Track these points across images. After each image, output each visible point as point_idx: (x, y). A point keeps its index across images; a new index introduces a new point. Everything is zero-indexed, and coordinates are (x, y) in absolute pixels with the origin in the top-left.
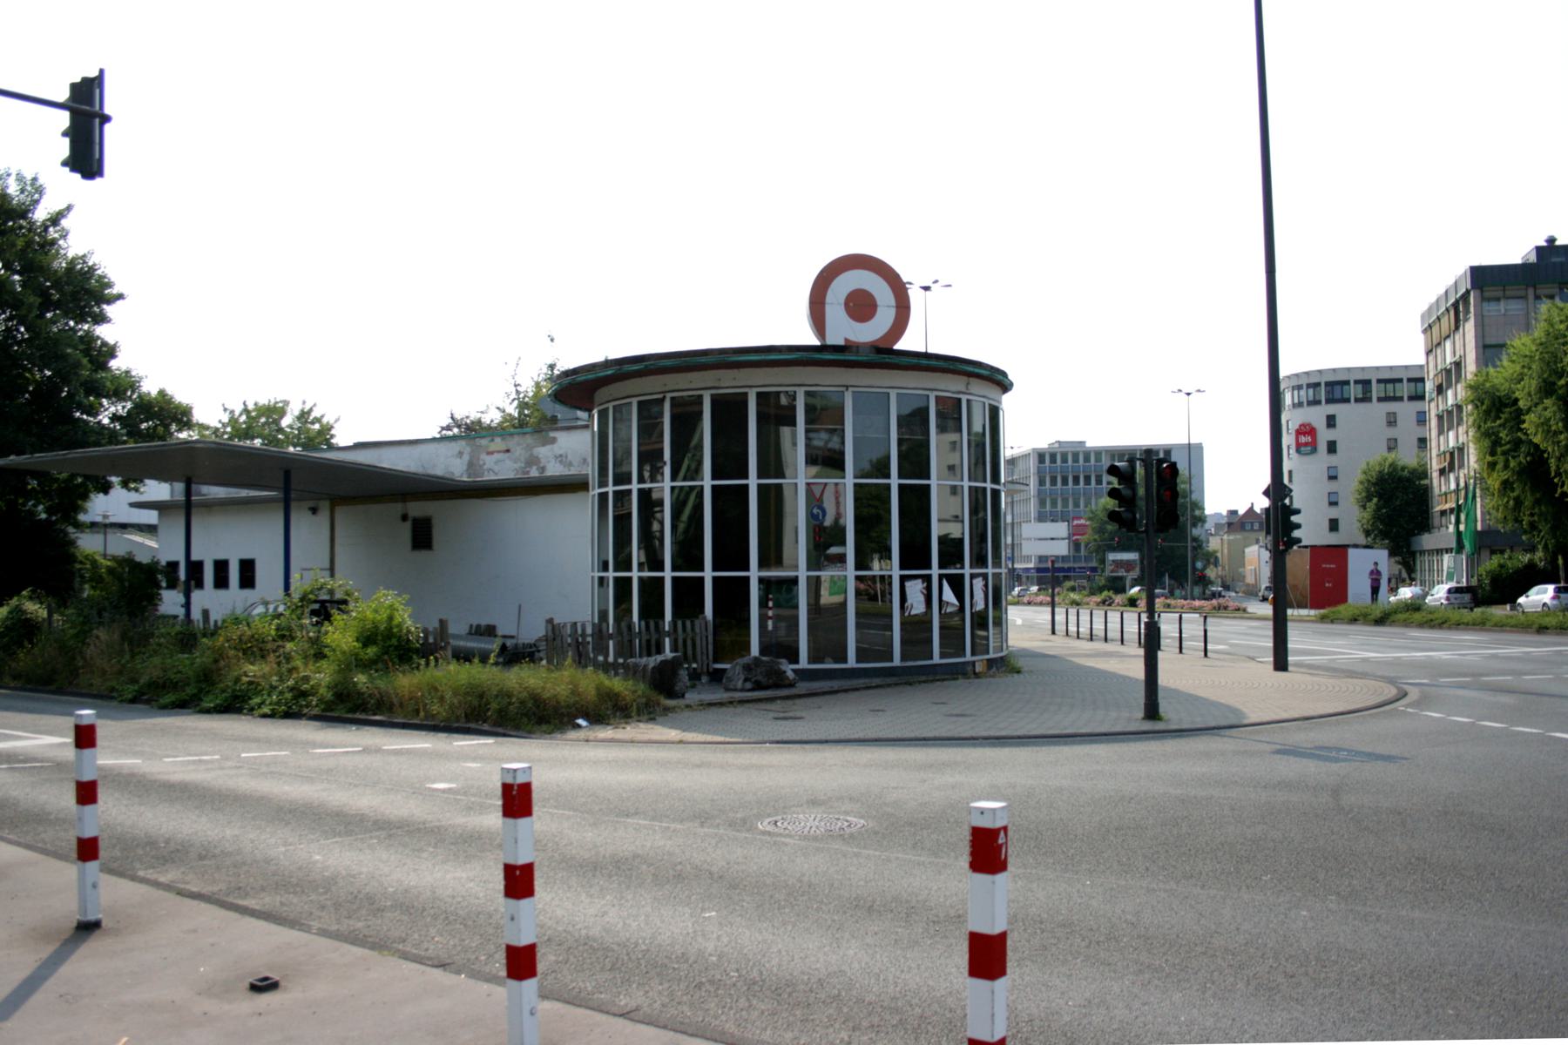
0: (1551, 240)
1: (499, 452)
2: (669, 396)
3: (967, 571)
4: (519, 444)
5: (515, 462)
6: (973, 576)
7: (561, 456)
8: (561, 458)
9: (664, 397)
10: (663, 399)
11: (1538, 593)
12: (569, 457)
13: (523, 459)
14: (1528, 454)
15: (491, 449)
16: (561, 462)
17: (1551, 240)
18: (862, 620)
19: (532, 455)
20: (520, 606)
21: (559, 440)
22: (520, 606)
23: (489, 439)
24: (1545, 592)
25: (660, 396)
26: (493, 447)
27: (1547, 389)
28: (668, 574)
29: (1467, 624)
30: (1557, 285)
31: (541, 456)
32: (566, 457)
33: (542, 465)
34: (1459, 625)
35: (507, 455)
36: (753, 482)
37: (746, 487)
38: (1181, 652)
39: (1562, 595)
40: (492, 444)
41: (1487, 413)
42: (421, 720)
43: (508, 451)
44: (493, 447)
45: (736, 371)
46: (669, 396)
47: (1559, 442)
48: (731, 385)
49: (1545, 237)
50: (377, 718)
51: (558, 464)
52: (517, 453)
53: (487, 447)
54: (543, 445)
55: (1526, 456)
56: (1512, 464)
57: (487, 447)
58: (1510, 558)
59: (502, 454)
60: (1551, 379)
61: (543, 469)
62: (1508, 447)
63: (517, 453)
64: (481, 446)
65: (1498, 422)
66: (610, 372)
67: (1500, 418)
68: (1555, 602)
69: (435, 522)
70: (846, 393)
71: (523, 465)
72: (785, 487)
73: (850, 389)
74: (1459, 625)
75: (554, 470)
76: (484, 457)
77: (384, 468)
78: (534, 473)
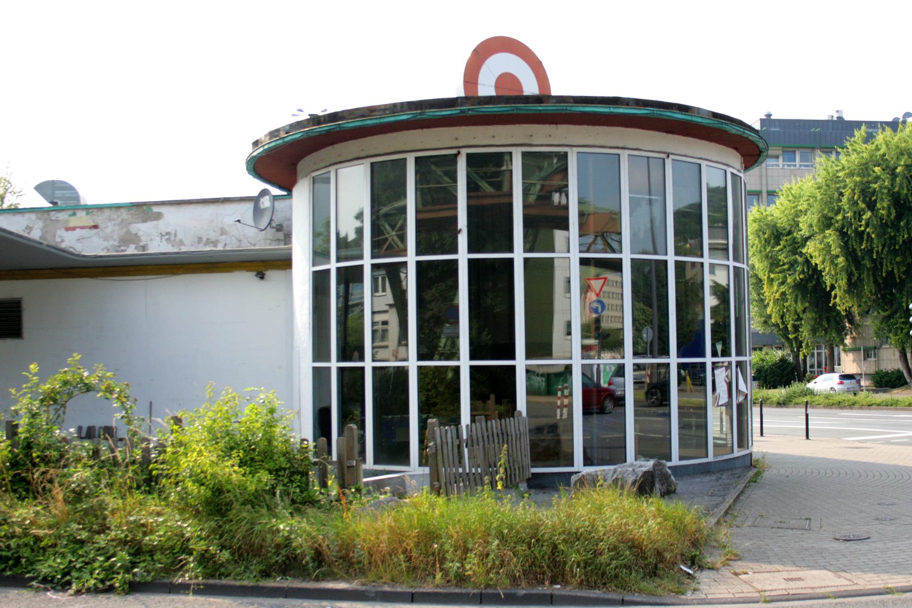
0: (769, 115)
1: (82, 228)
2: (464, 152)
3: (708, 360)
4: (110, 220)
5: (105, 240)
6: (715, 366)
7: (168, 233)
8: (167, 236)
9: (459, 152)
10: (456, 155)
11: (825, 380)
12: (179, 236)
13: (116, 237)
14: (803, 272)
15: (72, 225)
16: (168, 240)
17: (769, 115)
18: (638, 418)
19: (128, 232)
20: (151, 403)
21: (165, 215)
22: (151, 403)
23: (71, 212)
24: (831, 379)
25: (454, 151)
26: (73, 222)
27: (827, 222)
28: (673, 360)
29: (879, 405)
30: (781, 148)
31: (140, 233)
32: (176, 235)
33: (142, 244)
34: (871, 405)
35: (94, 231)
36: (519, 255)
37: (511, 262)
38: (807, 437)
39: (846, 381)
40: (73, 218)
41: (767, 241)
42: (437, 586)
43: (96, 227)
44: (73, 222)
45: (553, 127)
46: (464, 152)
47: (836, 265)
48: (545, 143)
49: (766, 113)
50: (342, 585)
51: (164, 243)
52: (108, 230)
53: (67, 221)
54: (145, 221)
55: (799, 275)
56: (789, 280)
57: (67, 221)
58: (767, 354)
59: (88, 230)
60: (830, 215)
61: (144, 248)
62: (786, 267)
63: (108, 230)
64: (57, 221)
65: (778, 248)
66: (404, 117)
67: (780, 244)
68: (840, 387)
69: (25, 306)
70: (666, 161)
71: (116, 243)
72: (557, 263)
73: (671, 157)
74: (852, 405)
75: (157, 247)
76: (61, 232)
77: (11, 233)
78: (131, 250)
